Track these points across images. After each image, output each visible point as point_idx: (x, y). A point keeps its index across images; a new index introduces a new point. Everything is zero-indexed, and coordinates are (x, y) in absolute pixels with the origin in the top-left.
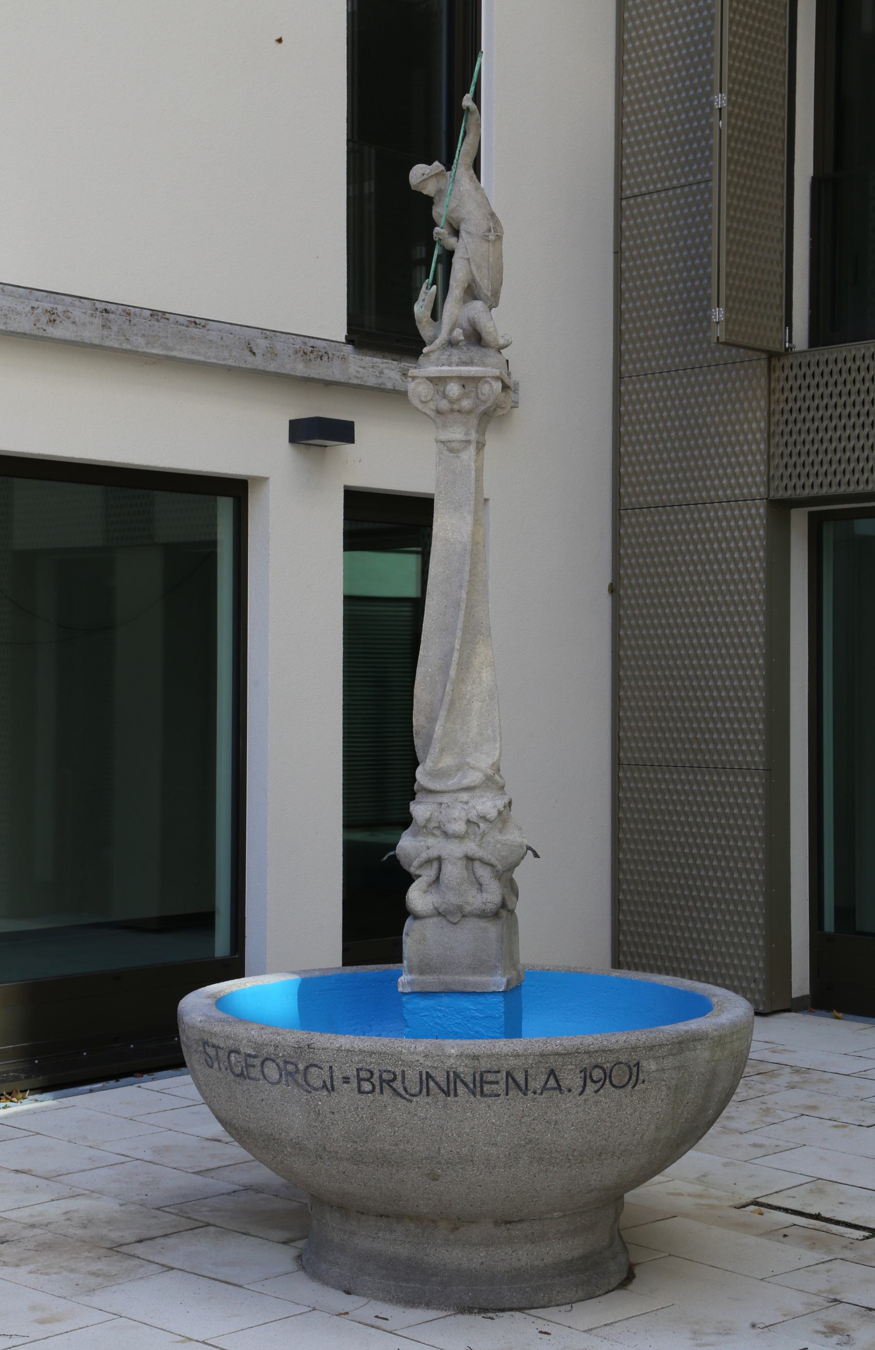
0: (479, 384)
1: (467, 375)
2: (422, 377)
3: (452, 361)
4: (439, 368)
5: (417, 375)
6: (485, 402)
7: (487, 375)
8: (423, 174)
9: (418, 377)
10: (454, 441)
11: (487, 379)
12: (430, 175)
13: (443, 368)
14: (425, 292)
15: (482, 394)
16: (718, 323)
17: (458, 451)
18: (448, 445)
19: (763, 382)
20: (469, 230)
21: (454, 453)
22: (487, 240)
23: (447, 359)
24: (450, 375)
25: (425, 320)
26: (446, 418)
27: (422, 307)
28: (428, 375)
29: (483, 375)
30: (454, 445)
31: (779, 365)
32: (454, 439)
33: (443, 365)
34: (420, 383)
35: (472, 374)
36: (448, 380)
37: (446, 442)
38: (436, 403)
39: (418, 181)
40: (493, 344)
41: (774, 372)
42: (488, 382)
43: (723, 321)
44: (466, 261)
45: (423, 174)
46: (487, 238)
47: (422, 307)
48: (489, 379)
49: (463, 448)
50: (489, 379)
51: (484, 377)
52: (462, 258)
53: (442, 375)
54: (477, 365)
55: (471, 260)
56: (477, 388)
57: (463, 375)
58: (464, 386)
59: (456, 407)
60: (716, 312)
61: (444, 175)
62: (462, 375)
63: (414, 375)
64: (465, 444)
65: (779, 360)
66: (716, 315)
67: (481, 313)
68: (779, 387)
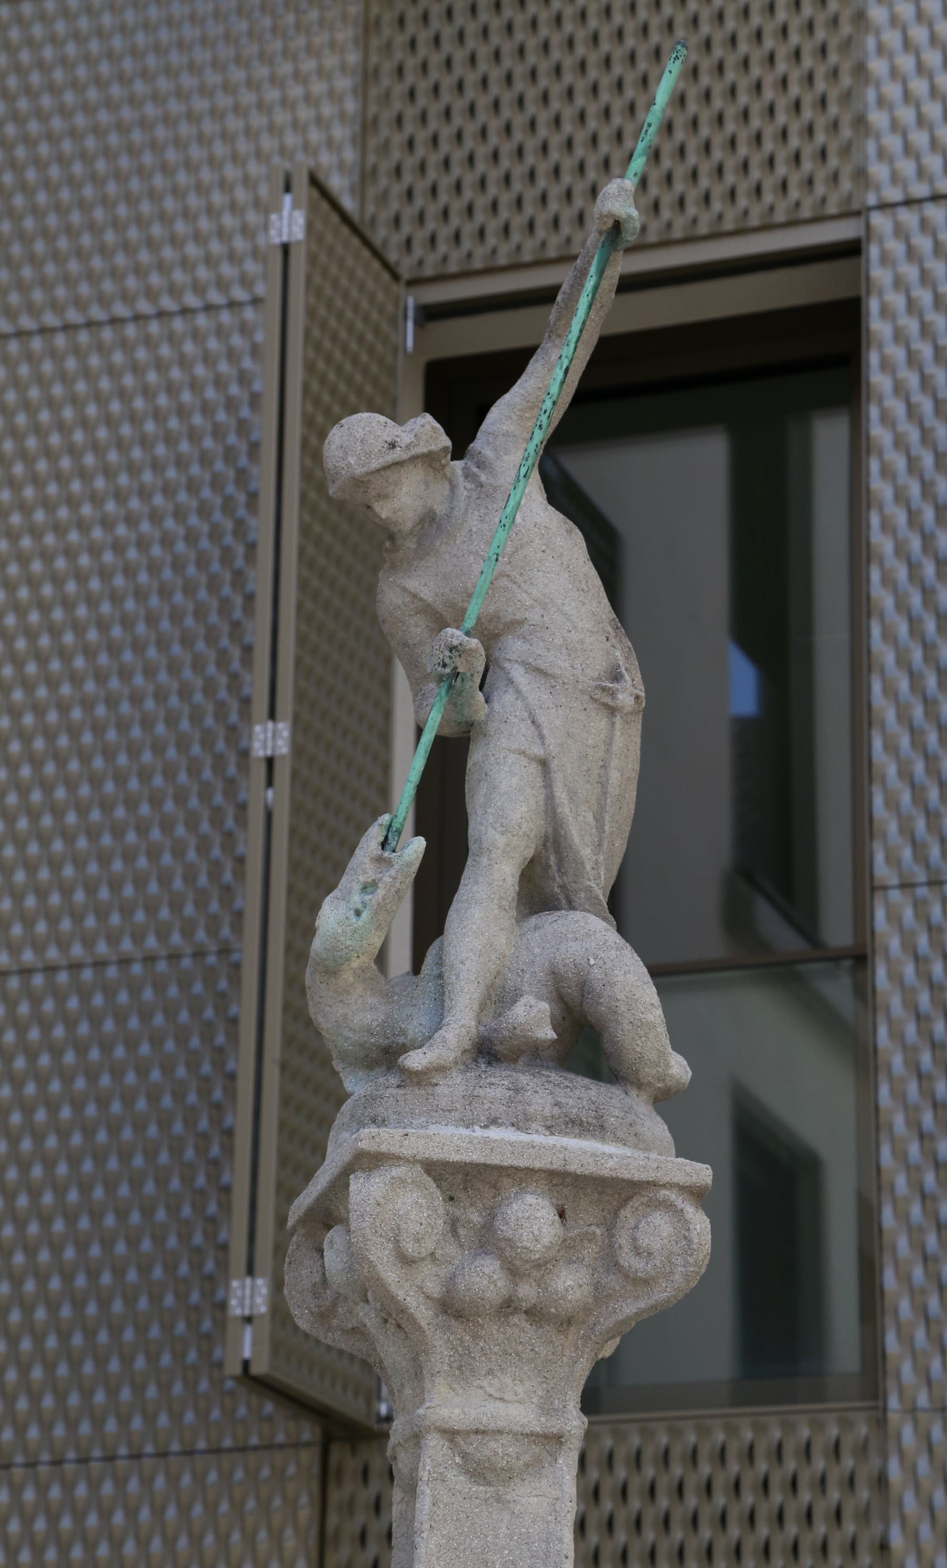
0: (625, 1213)
1: (591, 1168)
2: (412, 1161)
3: (531, 1109)
4: (479, 1132)
5: (395, 1150)
6: (647, 1282)
7: (667, 1179)
8: (393, 445)
9: (399, 1158)
10: (500, 1432)
11: (664, 1193)
12: (414, 451)
13: (494, 1133)
14: (379, 860)
15: (637, 1250)
16: (249, 1320)
17: (507, 1475)
18: (470, 1449)
19: (306, 1511)
20: (541, 664)
21: (488, 1483)
22: (605, 705)
23: (511, 1100)
24: (509, 1161)
25: (355, 964)
26: (475, 1337)
27: (358, 913)
28: (436, 1154)
29: (650, 1176)
30: (495, 1447)
31: (352, 1465)
32: (501, 1424)
33: (494, 1121)
34: (403, 1181)
35: (606, 1169)
36: (506, 1181)
37: (468, 1433)
38: (444, 1272)
39: (375, 464)
40: (648, 1073)
41: (339, 1482)
42: (669, 1206)
43: (262, 1316)
44: (534, 769)
45: (393, 445)
46: (608, 700)
47: (358, 913)
48: (672, 1195)
49: (527, 1466)
50: (672, 1195)
51: (654, 1185)
52: (523, 753)
53: (495, 1160)
54: (618, 1140)
55: (554, 765)
56: (610, 1227)
57: (573, 1168)
58: (562, 1214)
59: (527, 1292)
60: (243, 1287)
61: (443, 467)
62: (572, 1168)
63: (384, 1148)
64: (536, 1449)
65: (354, 1450)
66: (243, 1297)
67: (613, 954)
68: (353, 1526)
